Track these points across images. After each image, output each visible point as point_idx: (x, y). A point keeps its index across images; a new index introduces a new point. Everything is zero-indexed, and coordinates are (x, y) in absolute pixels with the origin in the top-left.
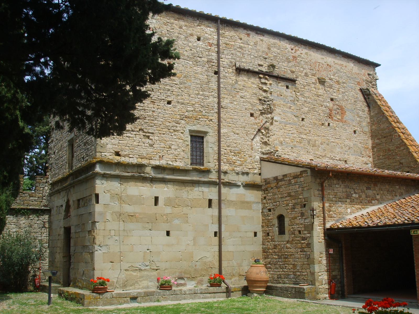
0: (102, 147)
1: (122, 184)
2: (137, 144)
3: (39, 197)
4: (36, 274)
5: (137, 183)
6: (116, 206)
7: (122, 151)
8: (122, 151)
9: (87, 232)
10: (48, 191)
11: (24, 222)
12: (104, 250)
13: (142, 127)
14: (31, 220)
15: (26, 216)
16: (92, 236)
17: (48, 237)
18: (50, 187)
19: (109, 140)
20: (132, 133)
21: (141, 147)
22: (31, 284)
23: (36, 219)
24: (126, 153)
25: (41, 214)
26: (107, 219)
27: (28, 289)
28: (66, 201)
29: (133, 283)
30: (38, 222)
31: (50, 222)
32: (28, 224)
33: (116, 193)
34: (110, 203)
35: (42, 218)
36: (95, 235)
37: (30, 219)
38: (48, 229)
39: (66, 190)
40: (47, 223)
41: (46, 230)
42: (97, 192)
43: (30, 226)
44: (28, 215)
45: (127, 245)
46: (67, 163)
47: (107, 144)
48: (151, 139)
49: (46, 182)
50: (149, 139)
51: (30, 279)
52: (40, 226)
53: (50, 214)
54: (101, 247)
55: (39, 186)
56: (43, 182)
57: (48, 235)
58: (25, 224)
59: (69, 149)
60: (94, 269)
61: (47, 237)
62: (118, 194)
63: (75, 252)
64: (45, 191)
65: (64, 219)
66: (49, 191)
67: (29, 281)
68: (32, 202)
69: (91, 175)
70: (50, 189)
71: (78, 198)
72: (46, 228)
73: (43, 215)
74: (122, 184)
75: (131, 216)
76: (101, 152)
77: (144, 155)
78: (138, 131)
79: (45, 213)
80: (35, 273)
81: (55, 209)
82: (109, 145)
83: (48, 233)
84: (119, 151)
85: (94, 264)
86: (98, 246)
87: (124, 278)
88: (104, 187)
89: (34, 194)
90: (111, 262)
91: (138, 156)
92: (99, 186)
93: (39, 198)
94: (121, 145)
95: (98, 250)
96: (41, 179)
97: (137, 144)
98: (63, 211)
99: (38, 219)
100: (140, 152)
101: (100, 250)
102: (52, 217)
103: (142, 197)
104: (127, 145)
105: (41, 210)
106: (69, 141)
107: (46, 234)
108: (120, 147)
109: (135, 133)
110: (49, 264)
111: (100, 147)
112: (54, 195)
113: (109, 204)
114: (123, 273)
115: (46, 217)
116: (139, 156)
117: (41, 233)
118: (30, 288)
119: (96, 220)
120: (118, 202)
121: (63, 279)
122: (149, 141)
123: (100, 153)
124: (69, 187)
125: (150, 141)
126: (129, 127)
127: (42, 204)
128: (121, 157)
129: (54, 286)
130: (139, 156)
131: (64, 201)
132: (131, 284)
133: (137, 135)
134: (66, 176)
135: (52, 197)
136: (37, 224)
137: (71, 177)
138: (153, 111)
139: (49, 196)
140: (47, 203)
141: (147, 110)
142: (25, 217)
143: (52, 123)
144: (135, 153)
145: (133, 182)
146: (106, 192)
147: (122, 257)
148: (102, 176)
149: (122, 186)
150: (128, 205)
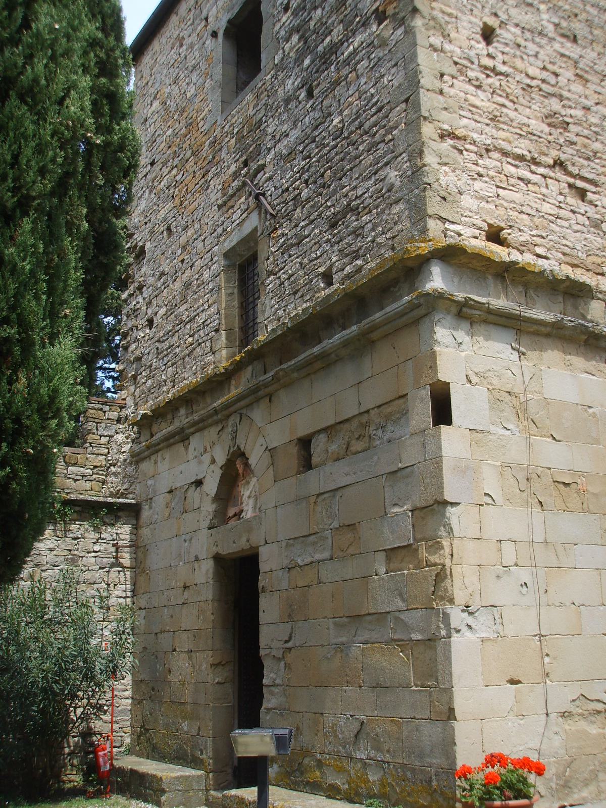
0: (444, 199)
1: (524, 354)
2: (552, 212)
3: (95, 467)
4: (89, 728)
5: (569, 357)
6: (512, 442)
7: (511, 227)
8: (511, 227)
9: (381, 556)
10: (126, 448)
11: (51, 546)
12: (483, 625)
13: (563, 157)
14: (75, 539)
15: (59, 526)
16: (416, 568)
17: (129, 600)
18: (133, 436)
19: (464, 181)
20: (533, 168)
21: (566, 224)
22: (75, 762)
23: (93, 535)
24: (525, 237)
25: (107, 520)
26: (486, 494)
27: (64, 782)
28: (221, 459)
29: (591, 771)
30: (97, 548)
31: (136, 546)
32: (66, 553)
33: (508, 388)
34: (492, 428)
35: (109, 533)
36: (448, 562)
37: (72, 535)
38: (128, 573)
39: (216, 423)
40: (126, 550)
41: (122, 574)
42: (443, 376)
43: (71, 559)
44: (66, 523)
45: (561, 605)
46: (223, 327)
47: (461, 194)
48: (591, 203)
49: (119, 421)
50: (583, 201)
51: (72, 744)
52: (104, 560)
53: (135, 522)
54: (471, 614)
55: (95, 431)
56: (108, 419)
57: (129, 594)
58: (54, 553)
59: (227, 281)
60: (451, 715)
61: (125, 598)
62: (515, 390)
63: (289, 645)
64: (114, 446)
65: (209, 529)
66: (129, 446)
67: (67, 750)
68: (75, 480)
69: (413, 307)
70: (133, 441)
71: (302, 432)
72: (124, 567)
73: (113, 525)
74: (524, 354)
75: (563, 483)
76: (444, 220)
77: (580, 254)
78: (549, 166)
79: (119, 517)
80: (88, 723)
81: (161, 500)
82: (469, 197)
83: (129, 587)
84: (503, 225)
85: (448, 691)
86: (463, 611)
87: (563, 751)
88: (467, 357)
89: (79, 456)
90: (513, 682)
91: (560, 255)
92: (446, 350)
93: (95, 471)
94: (505, 204)
95: (464, 629)
96: (101, 409)
97: (555, 211)
98: (209, 499)
99: (97, 536)
100: (564, 242)
101: (469, 627)
102: (145, 532)
103: (591, 411)
104: (524, 209)
105: (109, 506)
106: (226, 255)
107: (123, 587)
108: (501, 211)
109: (541, 170)
110: (133, 692)
111: (439, 199)
112: (153, 457)
113: (488, 432)
114: (556, 729)
115: (123, 531)
116: (564, 254)
117: (108, 585)
118: (73, 777)
119: (448, 497)
120: (518, 426)
121: (215, 751)
122: (588, 209)
123: (439, 222)
124: (242, 403)
125: (591, 211)
126: (523, 146)
127: (105, 490)
128: (511, 250)
129: (182, 777)
130: (564, 254)
131: (213, 461)
132: (586, 775)
133: (549, 181)
134: (222, 371)
135: (145, 466)
136: (93, 554)
137: (250, 368)
138: (587, 109)
139: (131, 463)
140: (122, 485)
141: (568, 99)
142: (54, 530)
143: (135, 237)
144: (551, 243)
145: (556, 352)
146: (474, 379)
147: (547, 660)
148: (454, 310)
149: (525, 363)
150: (550, 440)
